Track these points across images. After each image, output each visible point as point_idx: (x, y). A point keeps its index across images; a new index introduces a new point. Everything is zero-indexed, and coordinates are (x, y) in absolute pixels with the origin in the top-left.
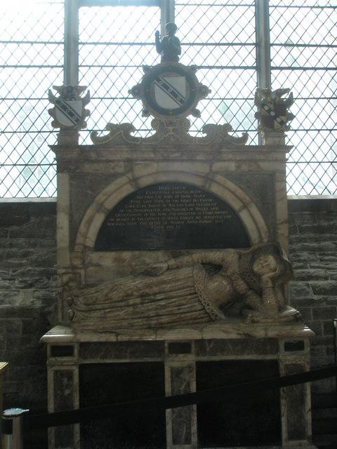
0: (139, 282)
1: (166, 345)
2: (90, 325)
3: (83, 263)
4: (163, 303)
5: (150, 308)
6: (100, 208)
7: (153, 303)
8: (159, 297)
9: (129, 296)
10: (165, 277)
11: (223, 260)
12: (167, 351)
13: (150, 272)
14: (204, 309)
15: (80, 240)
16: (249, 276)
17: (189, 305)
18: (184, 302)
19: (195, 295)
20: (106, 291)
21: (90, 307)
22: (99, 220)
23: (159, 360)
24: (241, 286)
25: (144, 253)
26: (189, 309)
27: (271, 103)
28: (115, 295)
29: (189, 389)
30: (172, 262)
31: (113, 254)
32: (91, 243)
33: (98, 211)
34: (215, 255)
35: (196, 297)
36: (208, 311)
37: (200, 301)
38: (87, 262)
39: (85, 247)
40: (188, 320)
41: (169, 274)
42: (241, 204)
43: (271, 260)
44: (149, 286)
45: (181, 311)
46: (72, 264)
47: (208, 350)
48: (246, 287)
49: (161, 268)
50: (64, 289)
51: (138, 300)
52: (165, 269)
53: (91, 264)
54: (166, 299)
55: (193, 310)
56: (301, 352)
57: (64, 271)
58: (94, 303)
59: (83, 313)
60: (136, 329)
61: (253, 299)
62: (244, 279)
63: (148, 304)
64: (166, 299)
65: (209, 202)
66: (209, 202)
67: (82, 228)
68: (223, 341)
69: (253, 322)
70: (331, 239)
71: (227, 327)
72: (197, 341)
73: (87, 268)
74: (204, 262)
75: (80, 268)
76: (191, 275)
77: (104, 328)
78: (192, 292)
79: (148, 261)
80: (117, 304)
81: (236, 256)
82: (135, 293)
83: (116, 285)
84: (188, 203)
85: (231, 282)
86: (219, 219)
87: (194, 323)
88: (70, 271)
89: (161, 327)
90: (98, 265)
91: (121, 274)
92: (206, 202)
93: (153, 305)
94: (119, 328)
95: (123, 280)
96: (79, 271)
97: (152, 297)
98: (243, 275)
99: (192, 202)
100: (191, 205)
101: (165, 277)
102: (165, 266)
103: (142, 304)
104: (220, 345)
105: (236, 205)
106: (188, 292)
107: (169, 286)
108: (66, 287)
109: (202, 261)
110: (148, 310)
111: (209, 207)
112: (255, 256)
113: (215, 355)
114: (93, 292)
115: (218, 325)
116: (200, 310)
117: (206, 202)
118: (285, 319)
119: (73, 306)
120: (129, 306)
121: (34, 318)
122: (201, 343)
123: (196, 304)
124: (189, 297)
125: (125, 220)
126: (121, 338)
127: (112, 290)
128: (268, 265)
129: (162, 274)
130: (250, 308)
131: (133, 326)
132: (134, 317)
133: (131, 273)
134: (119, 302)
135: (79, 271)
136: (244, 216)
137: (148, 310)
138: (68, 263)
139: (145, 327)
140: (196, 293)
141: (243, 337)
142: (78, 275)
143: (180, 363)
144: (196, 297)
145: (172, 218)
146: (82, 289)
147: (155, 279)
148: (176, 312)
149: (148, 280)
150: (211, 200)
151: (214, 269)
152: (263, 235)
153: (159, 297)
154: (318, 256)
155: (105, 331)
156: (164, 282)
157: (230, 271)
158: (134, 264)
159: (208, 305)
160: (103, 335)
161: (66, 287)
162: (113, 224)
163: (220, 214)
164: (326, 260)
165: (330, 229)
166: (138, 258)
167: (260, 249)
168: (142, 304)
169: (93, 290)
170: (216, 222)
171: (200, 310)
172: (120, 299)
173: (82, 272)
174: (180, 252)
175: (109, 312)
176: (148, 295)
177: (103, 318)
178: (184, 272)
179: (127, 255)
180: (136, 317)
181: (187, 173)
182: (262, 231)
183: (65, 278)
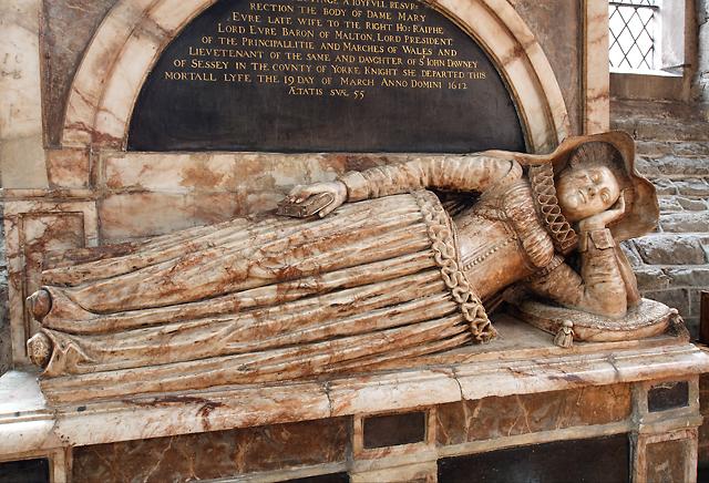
0: (271, 234)
1: (358, 424)
2: (110, 382)
3: (93, 181)
4: (343, 298)
5: (305, 314)
6: (142, 24)
7: (314, 301)
8: (330, 281)
9: (238, 280)
10: (341, 222)
11: (485, 179)
12: (358, 441)
13: (292, 210)
14: (458, 311)
15: (77, 112)
17: (422, 303)
18: (405, 293)
19: (435, 274)
20: (165, 267)
21: (112, 320)
22: (139, 60)
23: (334, 468)
25: (270, 158)
26: (419, 315)
28: (194, 280)
29: (116, 139)
30: (356, 181)
31: (184, 160)
32: (115, 122)
33: (136, 31)
34: (464, 168)
35: (441, 278)
36: (469, 318)
37: (446, 289)
38: (101, 180)
39: (96, 136)
40: (418, 344)
41: (356, 213)
42: (510, 45)
43: (608, 179)
44: (299, 249)
45: (398, 320)
46: (52, 185)
47: (468, 423)
48: (551, 248)
49: (330, 197)
50: (29, 261)
51: (270, 293)
52: (339, 199)
53: (115, 187)
54: (351, 286)
55: (431, 315)
56: (681, 411)
57: (26, 207)
58: (125, 307)
59: (86, 342)
60: (267, 385)
61: (562, 279)
62: (544, 226)
63: (299, 303)
64: (351, 286)
65: (435, 36)
66: (435, 36)
67: (86, 78)
68: (510, 400)
69: (577, 339)
71: (517, 357)
72: (442, 408)
73: (107, 196)
74: (437, 183)
75: (81, 200)
76: (417, 216)
77: (161, 388)
78: (429, 263)
79: (282, 180)
80: (206, 306)
81: (517, 171)
82: (257, 271)
83: (196, 248)
84: (384, 33)
86: (459, 80)
87: (431, 353)
88: (48, 206)
89: (342, 370)
90: (138, 191)
91: (209, 217)
92: (427, 35)
93: (319, 305)
94: (210, 384)
95: (215, 233)
96: (76, 207)
97: (312, 282)
99: (394, 32)
100: (391, 39)
101: (341, 222)
102: (337, 191)
103: (279, 302)
104: (499, 409)
105: (499, 47)
106: (413, 266)
107: (360, 246)
108: (37, 256)
109: (431, 179)
110: (303, 322)
111: (436, 49)
112: (563, 165)
113: (485, 438)
114: (123, 268)
115: (494, 355)
116: (446, 315)
117: (427, 35)
118: (651, 329)
119: (50, 319)
120: (244, 310)
122: (450, 413)
123: (439, 298)
124: (420, 278)
125: (217, 65)
126: (216, 419)
127: (183, 263)
128: (603, 192)
129: (334, 213)
130: (550, 300)
131: (256, 374)
132: (257, 344)
133: (237, 213)
134: (209, 297)
135: (76, 207)
136: (516, 73)
137: (303, 322)
138: (40, 184)
139: (293, 374)
140: (437, 267)
141: (564, 385)
142: (76, 221)
143: (395, 471)
144: (441, 278)
145: (343, 70)
146: (84, 260)
147: (315, 228)
148: (381, 325)
149: (293, 231)
150: (439, 30)
151: (460, 200)
152: (558, 123)
153: (330, 281)
155: (166, 399)
156: (344, 238)
158: (242, 187)
159: (469, 301)
160: (158, 412)
161: (37, 256)
162: (183, 76)
163: (459, 69)
166: (255, 172)
168: (279, 302)
169: (123, 263)
170: (452, 86)
171: (446, 315)
172: (208, 290)
173: (89, 211)
174: (366, 159)
175: (176, 332)
176: (296, 275)
177: (156, 355)
178: (397, 210)
179: (222, 163)
180: (265, 343)
181: (32, 412)
182: (555, 113)
183: (34, 229)
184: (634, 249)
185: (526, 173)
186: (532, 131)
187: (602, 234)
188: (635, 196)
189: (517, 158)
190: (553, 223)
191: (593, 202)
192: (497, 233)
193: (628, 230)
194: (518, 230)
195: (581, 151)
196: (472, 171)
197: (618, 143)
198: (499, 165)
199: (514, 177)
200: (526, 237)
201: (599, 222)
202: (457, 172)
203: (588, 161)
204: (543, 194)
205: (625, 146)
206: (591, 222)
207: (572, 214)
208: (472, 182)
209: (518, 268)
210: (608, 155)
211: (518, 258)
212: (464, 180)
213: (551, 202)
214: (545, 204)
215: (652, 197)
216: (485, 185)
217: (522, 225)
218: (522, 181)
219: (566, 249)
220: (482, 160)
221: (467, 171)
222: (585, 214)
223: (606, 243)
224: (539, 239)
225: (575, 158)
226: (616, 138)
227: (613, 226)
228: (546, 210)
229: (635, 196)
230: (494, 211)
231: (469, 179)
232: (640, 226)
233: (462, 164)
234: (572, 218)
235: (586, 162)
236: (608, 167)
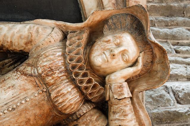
11: (29, 42)
16: (85, 75)
24: (69, 97)
27: (20, 93)
43: (128, 43)
70: (184, 24)
81: (57, 35)
85: (42, 81)
98: (70, 74)
112: (95, 33)
121: (58, 70)
128: (123, 53)
154: (172, 47)
157: (44, 63)
164: (183, 52)
165: (182, 12)
167: (104, 22)
184: (171, 94)
185: (65, 37)
186: (86, 6)
187: (121, 87)
188: (153, 57)
189: (58, 25)
190: (80, 78)
191: (115, 60)
192: (29, 86)
193: (147, 83)
194: (47, 84)
195: (110, 21)
196: (17, 35)
197: (139, 16)
198: (40, 30)
199: (52, 40)
200: (53, 90)
201: (118, 79)
202: (5, 35)
203: (115, 29)
204: (72, 54)
205: (143, 17)
206: (113, 77)
207: (98, 71)
208: (19, 45)
209: (48, 115)
210: (132, 24)
211: (46, 107)
212: (11, 42)
213: (79, 61)
214: (74, 63)
215: (164, 57)
216: (29, 46)
217: (49, 80)
218: (60, 44)
219: (95, 97)
220: (28, 27)
221: (13, 35)
222: (108, 71)
223: (123, 94)
224: (64, 91)
225: (106, 26)
226: (137, 11)
227: (129, 81)
228: (74, 67)
229: (153, 57)
230: (29, 69)
231: (15, 41)
232: (157, 79)
233: (10, 29)
234: (99, 76)
235: (114, 29)
236: (131, 34)
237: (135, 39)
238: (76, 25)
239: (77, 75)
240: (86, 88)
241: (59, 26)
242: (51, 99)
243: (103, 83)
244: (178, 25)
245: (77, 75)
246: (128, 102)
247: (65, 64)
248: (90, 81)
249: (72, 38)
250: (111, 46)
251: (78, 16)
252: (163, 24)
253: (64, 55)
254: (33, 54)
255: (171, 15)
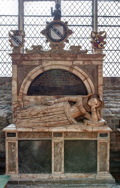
16: (87, 106)
24: (83, 110)
43: (96, 100)
81: (82, 99)
85: (78, 107)
98: (84, 106)
112: (89, 98)
128: (94, 102)
157: (79, 104)
164: (117, 100)
185: (83, 98)
187: (94, 109)
201: (93, 107)
209: (80, 114)
219: (89, 111)
237: (97, 99)
238: (53, 152)
239: (85, 106)
240: (87, 109)
241: (82, 97)
242: (32, 132)
243: (90, 108)
244: (117, 93)
245: (85, 106)
246: (95, 112)
247: (83, 104)
248: (88, 108)
249: (85, 99)
250: (92, 101)
251: (86, 93)
252: (112, 92)
253: (83, 103)
254: (77, 102)
255: (116, 90)
